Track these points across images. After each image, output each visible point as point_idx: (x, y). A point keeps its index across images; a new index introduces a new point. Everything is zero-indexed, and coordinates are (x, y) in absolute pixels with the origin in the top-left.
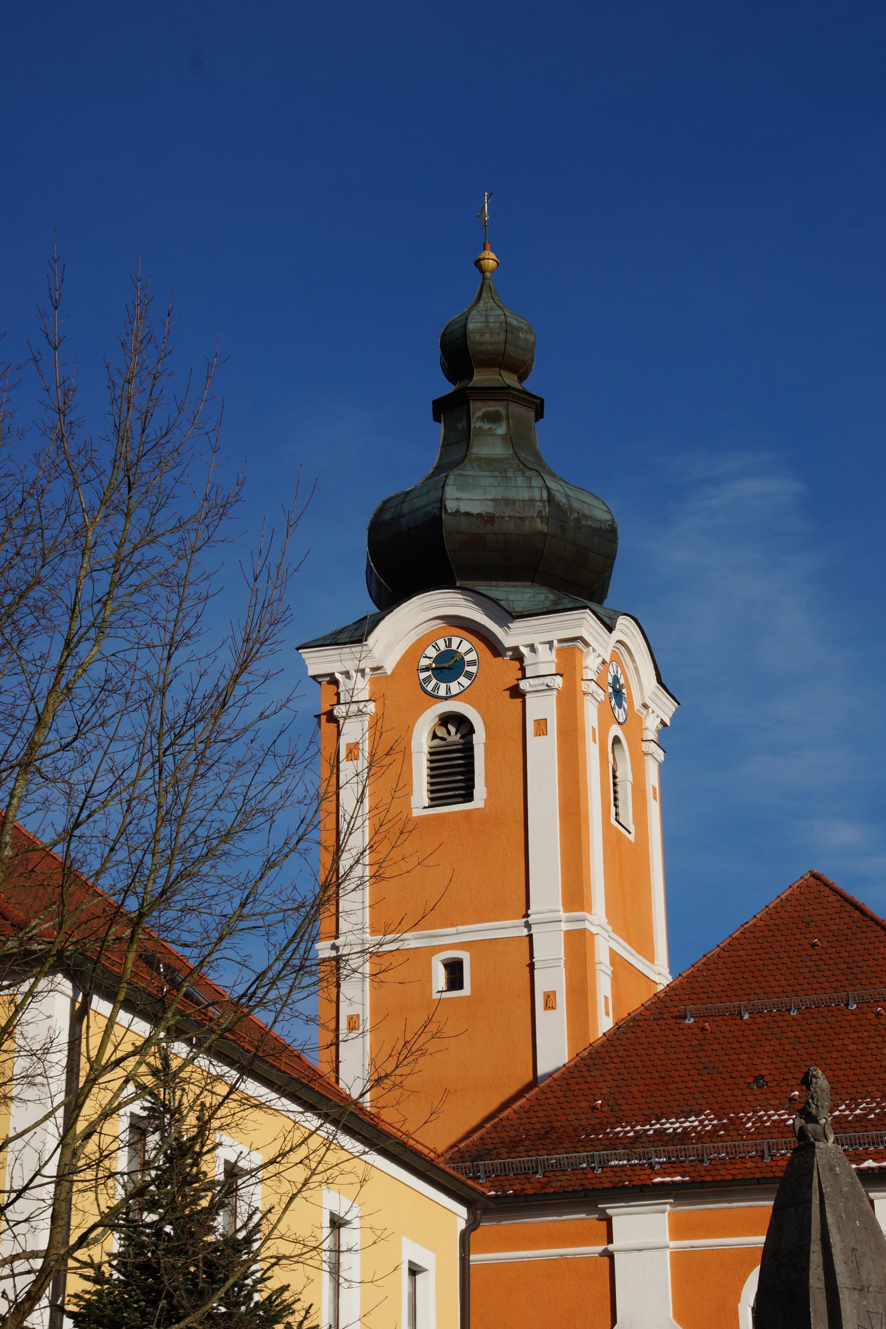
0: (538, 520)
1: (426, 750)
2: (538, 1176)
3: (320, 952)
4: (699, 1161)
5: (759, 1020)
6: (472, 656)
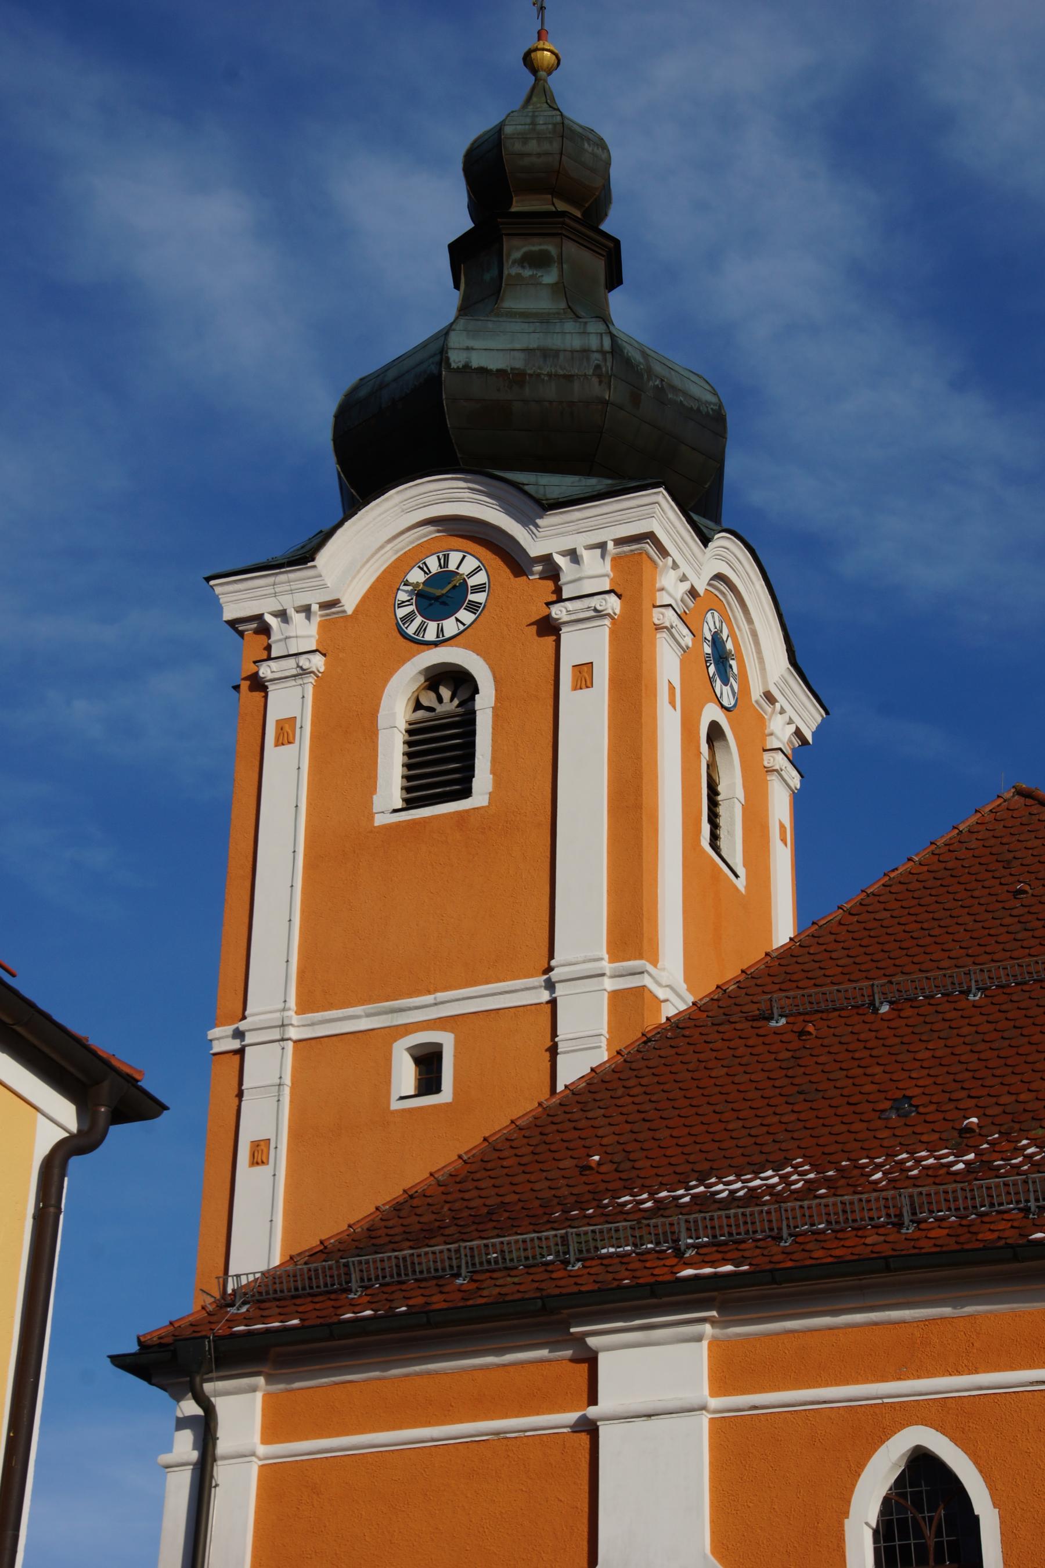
0: (595, 380)
1: (403, 726)
2: (459, 1281)
3: (215, 1043)
4: (774, 1238)
5: (908, 1012)
6: (481, 578)
